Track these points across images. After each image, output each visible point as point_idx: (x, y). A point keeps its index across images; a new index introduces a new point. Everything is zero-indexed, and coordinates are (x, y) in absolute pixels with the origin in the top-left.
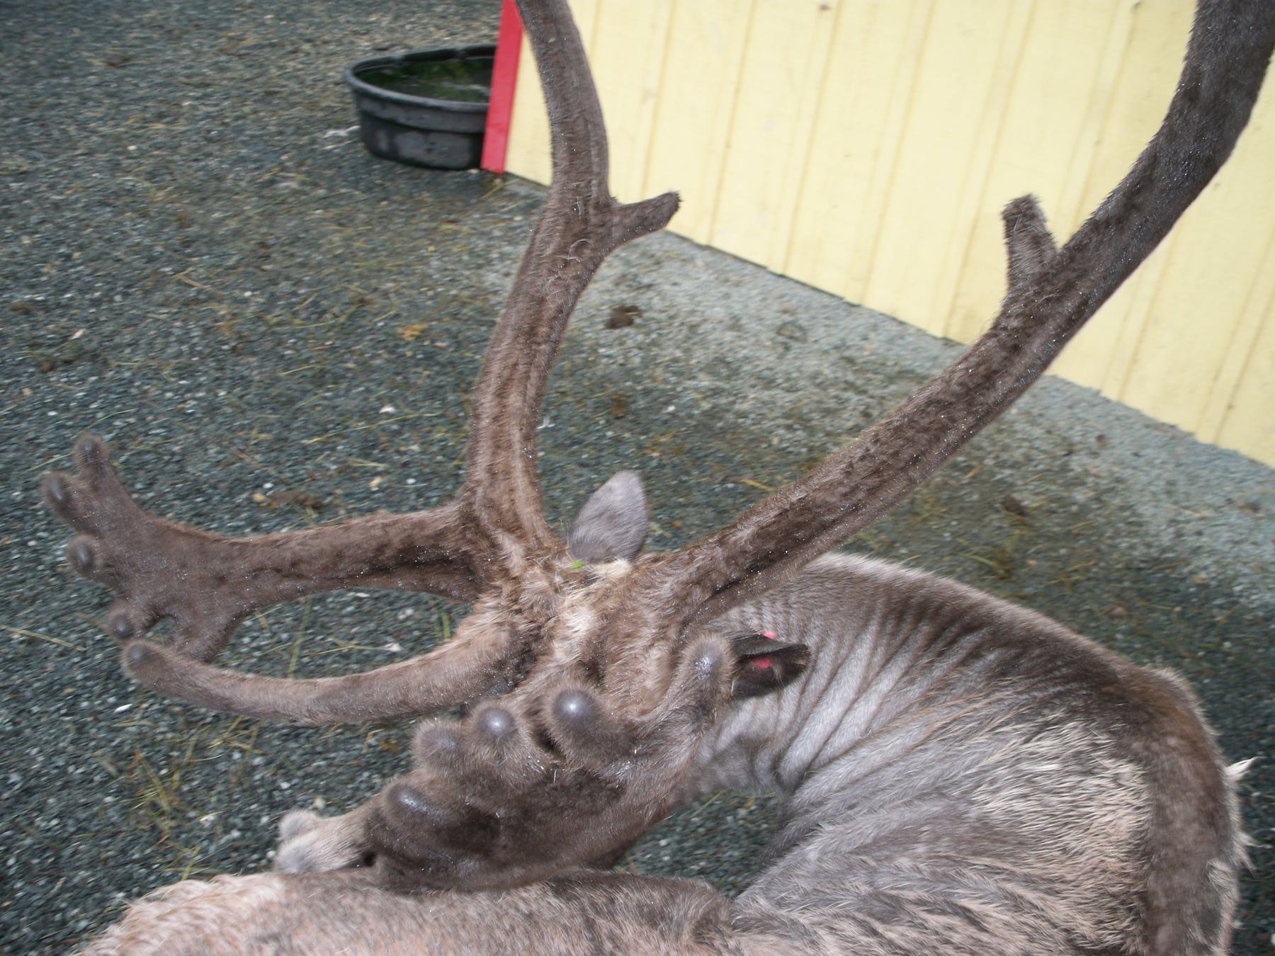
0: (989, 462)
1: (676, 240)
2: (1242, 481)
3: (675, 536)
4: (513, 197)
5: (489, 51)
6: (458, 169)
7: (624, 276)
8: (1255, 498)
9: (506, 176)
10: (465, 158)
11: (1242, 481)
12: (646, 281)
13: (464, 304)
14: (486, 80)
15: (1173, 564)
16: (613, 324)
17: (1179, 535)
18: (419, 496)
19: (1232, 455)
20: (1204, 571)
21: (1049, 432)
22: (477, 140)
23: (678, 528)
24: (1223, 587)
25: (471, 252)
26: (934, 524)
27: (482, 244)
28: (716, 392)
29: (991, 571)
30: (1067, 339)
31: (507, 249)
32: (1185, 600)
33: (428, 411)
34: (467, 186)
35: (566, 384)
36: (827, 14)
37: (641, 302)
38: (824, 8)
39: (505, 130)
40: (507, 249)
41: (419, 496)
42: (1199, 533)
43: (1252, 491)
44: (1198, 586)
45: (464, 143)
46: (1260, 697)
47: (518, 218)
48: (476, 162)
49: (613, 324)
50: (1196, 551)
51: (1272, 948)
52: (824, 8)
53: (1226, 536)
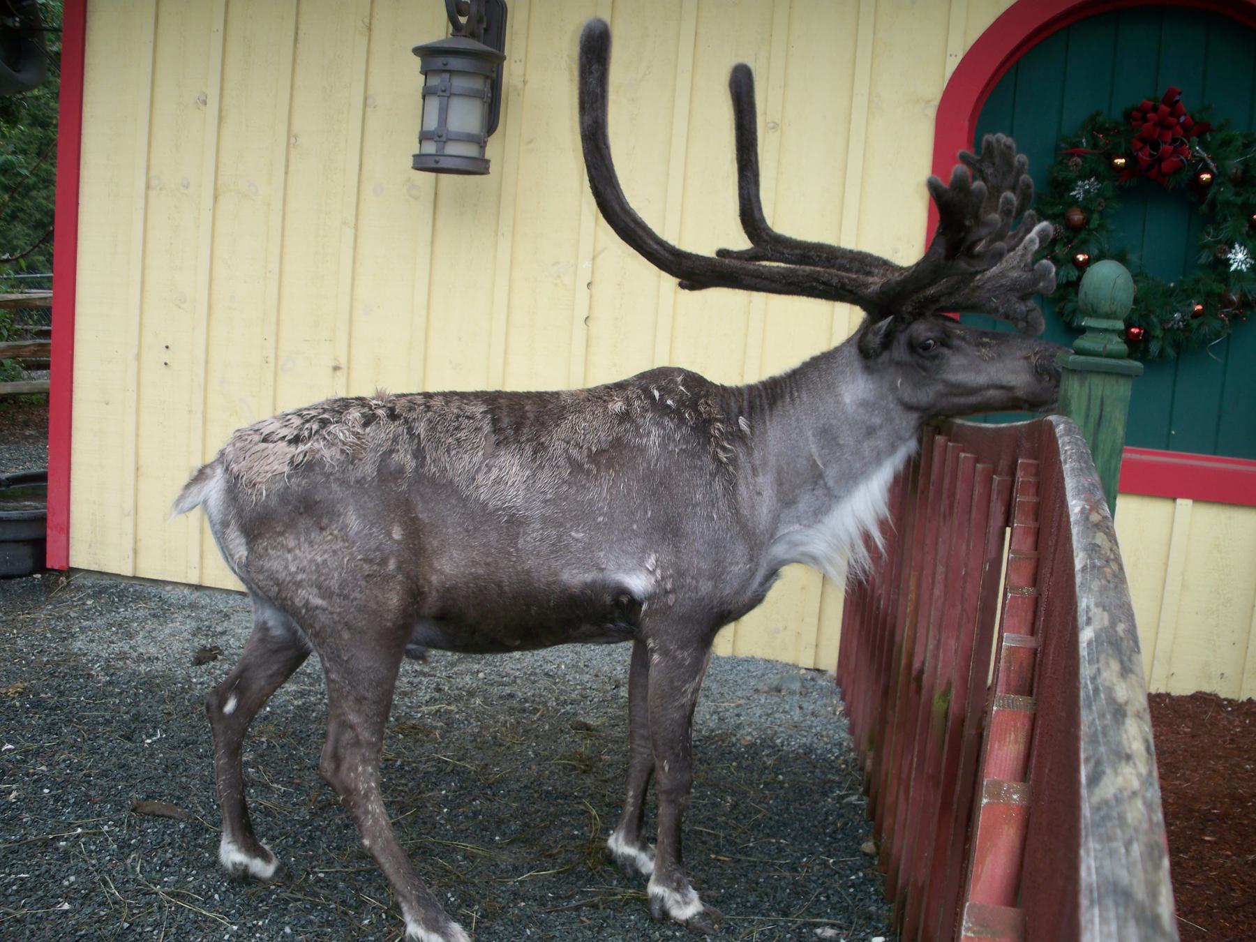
0: (552, 703)
1: (237, 597)
2: (763, 675)
3: (297, 789)
4: (79, 588)
5: (42, 477)
6: (21, 576)
7: (199, 628)
8: (775, 683)
9: (71, 571)
10: (29, 563)
11: (763, 675)
12: (219, 629)
13: (58, 665)
14: (41, 495)
15: (723, 738)
16: (199, 661)
17: (721, 720)
18: (56, 801)
19: (750, 661)
20: (748, 736)
21: (596, 676)
22: (39, 545)
23: (298, 784)
24: (767, 742)
25: (53, 630)
26: (517, 749)
27: (61, 625)
28: (302, 694)
29: (574, 768)
30: (541, 399)
31: (85, 623)
32: (738, 757)
33: (46, 742)
34: (33, 588)
35: (169, 707)
36: (339, 373)
37: (220, 642)
38: (336, 368)
39: (66, 530)
40: (85, 623)
41: (56, 801)
42: (738, 715)
43: (773, 679)
44: (746, 746)
45: (25, 551)
46: (816, 803)
47: (89, 602)
48: (40, 564)
49: (199, 661)
50: (739, 726)
51: (454, 9)
52: (336, 368)
53: (759, 712)
